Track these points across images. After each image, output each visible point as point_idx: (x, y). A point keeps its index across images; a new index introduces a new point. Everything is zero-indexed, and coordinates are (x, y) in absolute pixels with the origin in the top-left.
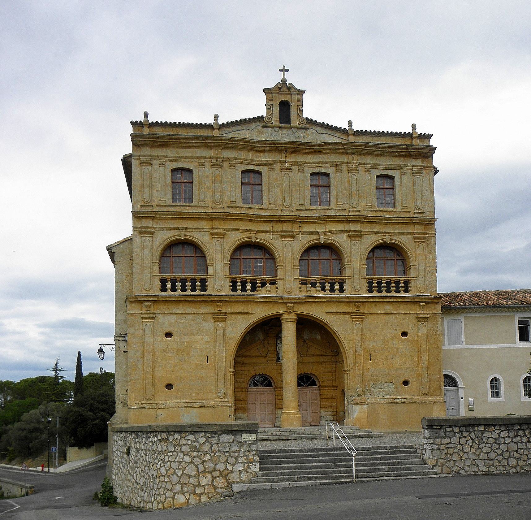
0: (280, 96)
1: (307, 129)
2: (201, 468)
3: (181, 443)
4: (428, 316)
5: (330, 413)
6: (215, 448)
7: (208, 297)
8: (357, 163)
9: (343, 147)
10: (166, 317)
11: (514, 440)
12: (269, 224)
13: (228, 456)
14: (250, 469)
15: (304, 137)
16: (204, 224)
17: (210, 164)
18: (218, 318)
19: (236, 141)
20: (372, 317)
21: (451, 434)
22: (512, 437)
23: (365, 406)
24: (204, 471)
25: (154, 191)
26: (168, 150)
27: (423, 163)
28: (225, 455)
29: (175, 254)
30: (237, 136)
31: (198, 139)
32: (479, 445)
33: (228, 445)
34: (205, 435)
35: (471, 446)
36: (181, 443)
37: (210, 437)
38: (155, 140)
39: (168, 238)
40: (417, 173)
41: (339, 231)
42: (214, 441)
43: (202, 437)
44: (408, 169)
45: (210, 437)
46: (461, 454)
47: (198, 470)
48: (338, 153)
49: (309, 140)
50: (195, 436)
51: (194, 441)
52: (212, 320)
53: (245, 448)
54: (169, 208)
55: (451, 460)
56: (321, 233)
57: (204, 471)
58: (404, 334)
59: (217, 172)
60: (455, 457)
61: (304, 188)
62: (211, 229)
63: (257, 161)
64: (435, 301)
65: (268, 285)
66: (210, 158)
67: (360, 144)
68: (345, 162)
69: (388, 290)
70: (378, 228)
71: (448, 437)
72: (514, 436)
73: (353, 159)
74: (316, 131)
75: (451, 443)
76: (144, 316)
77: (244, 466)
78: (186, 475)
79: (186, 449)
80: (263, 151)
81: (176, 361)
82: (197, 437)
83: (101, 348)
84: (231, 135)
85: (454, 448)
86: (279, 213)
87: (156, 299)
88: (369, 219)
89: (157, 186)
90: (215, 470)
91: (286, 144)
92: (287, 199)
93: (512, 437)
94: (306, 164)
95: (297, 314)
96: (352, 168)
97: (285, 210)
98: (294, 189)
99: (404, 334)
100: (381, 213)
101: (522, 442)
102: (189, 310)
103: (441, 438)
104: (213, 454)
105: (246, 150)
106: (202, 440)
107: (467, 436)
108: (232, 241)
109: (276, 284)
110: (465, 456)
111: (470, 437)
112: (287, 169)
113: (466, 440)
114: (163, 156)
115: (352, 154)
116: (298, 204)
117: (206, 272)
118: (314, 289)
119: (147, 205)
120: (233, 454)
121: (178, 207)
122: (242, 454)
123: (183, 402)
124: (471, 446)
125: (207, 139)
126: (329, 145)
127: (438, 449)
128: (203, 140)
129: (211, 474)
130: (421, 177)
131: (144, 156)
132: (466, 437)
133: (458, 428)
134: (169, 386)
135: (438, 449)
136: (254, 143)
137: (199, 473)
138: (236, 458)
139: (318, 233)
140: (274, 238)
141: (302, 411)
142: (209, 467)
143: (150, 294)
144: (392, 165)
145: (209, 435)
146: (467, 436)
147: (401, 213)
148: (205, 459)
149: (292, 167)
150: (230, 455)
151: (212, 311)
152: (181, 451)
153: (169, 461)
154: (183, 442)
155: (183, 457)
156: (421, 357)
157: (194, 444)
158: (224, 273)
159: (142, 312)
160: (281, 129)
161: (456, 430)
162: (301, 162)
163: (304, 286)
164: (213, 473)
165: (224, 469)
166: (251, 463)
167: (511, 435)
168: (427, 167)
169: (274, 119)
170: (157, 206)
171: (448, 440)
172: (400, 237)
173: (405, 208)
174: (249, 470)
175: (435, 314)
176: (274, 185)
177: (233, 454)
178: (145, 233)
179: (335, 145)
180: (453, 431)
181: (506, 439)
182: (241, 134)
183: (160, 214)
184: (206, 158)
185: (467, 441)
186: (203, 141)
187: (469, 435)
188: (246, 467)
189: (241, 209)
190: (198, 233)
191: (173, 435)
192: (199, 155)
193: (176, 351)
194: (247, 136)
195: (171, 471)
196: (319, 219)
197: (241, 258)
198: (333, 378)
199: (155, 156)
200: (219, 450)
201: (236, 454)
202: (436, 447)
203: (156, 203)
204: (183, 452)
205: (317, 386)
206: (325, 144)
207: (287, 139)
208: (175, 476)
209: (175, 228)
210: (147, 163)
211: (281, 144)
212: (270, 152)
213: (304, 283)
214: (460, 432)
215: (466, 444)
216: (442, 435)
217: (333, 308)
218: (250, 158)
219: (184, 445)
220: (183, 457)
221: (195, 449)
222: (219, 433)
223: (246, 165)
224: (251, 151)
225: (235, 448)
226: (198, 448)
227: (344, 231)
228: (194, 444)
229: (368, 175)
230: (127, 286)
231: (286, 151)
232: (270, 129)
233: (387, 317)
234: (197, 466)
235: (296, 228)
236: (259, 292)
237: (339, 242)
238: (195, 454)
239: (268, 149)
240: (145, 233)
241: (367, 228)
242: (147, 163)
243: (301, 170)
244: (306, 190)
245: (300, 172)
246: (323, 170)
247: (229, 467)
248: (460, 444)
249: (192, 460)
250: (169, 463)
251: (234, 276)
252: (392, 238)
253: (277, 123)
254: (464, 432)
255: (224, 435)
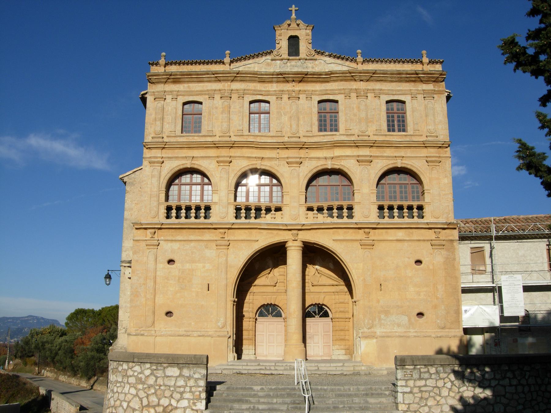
0: (289, 31)
1: (316, 60)
2: (145, 402)
3: (128, 374)
4: (444, 243)
5: (342, 347)
6: (160, 381)
7: (211, 224)
8: (366, 89)
9: (350, 75)
10: (170, 244)
11: (501, 383)
12: (275, 151)
13: (173, 390)
14: (196, 406)
15: (313, 68)
16: (212, 152)
17: (373, 95)
18: (221, 245)
19: (244, 74)
20: (383, 244)
21: (426, 376)
22: (499, 380)
23: (375, 340)
24: (148, 406)
25: (165, 123)
26: (180, 86)
27: (434, 88)
28: (169, 389)
29: (320, 183)
30: (247, 69)
31: (208, 74)
32: (459, 388)
33: (174, 379)
34: (151, 366)
35: (450, 390)
36: (128, 374)
37: (155, 370)
38: (168, 77)
39: (176, 167)
40: (428, 97)
41: (347, 156)
42: (160, 373)
43: (148, 368)
44: (419, 94)
45: (155, 370)
46: (438, 398)
47: (142, 404)
48: (346, 80)
49: (317, 69)
50: (141, 367)
51: (140, 373)
52: (215, 247)
53: (191, 383)
54: (178, 138)
55: (426, 405)
56: (328, 158)
57: (148, 406)
58: (419, 262)
59: (226, 104)
60: (431, 402)
61: (312, 115)
62: (218, 157)
63: (265, 91)
64: (451, 227)
65: (273, 212)
66: (220, 90)
67: (367, 72)
68: (353, 89)
69: (178, 217)
70: (388, 152)
71: (422, 379)
72: (501, 378)
73: (362, 85)
74: (325, 61)
75: (426, 386)
76: (149, 243)
77: (189, 403)
78: (131, 408)
79: (132, 380)
80: (271, 82)
81: (177, 289)
82: (143, 368)
83: (108, 273)
84: (241, 69)
85: (429, 392)
86: (286, 139)
87: (159, 226)
88: (378, 143)
89: (168, 118)
90: (158, 405)
91: (293, 74)
92: (294, 126)
93: (499, 380)
94: (313, 92)
95: (303, 242)
96: (294, 97)
97: (291, 137)
98: (301, 117)
99: (419, 262)
100: (392, 137)
101: (511, 385)
102: (192, 238)
103: (415, 380)
104: (157, 387)
105: (254, 81)
106: (148, 372)
107: (445, 378)
108: (238, 169)
109: (281, 211)
110: (443, 401)
111: (449, 379)
112: (294, 97)
113: (444, 382)
114: (175, 91)
115: (361, 80)
116: (305, 130)
117: (353, 200)
118: (322, 215)
119: (158, 136)
120: (178, 389)
121: (187, 137)
122: (188, 389)
123: (181, 331)
124: (450, 390)
125: (216, 74)
126: (176, 75)
127: (411, 392)
128: (214, 74)
129: (154, 408)
130: (432, 101)
131: (158, 92)
132: (444, 379)
133: (434, 369)
134: (169, 314)
135: (411, 392)
136: (262, 75)
137: (143, 407)
138: (182, 393)
139: (326, 158)
140: (280, 165)
141: (313, 343)
142: (153, 401)
143: (156, 221)
144: (402, 90)
145: (154, 367)
146: (445, 378)
147: (413, 137)
148: (150, 393)
149: (301, 96)
150: (175, 390)
151: (215, 238)
152: (128, 383)
153: (117, 392)
154: (130, 373)
155: (129, 389)
156: (437, 287)
157: (140, 376)
158: (228, 201)
159: (146, 239)
160: (289, 61)
161: (433, 370)
162: (308, 91)
163: (310, 212)
164: (157, 408)
165: (168, 405)
166: (196, 399)
167: (498, 376)
168: (438, 91)
169: (283, 52)
170: (168, 137)
171: (422, 383)
172: (413, 161)
173: (417, 131)
174: (194, 408)
175: (452, 241)
176: (281, 114)
177: (178, 389)
178: (154, 162)
179: (342, 73)
180: (428, 371)
181: (492, 381)
182: (250, 68)
183: (169, 145)
184: (215, 90)
185: (445, 383)
186: (213, 76)
187: (447, 377)
188: (191, 404)
189: (247, 137)
190: (205, 161)
191: (122, 365)
192: (209, 88)
193: (177, 278)
194: (256, 69)
195: (118, 403)
196: (326, 144)
197: (386, 183)
198: (250, 309)
199: (370, 90)
200: (164, 384)
201: (182, 389)
202: (408, 390)
203: (167, 134)
204: (129, 384)
205: (258, 316)
206: (331, 73)
207: (295, 70)
208: (121, 408)
209: (183, 157)
210: (160, 98)
211: (288, 74)
212: (278, 82)
213: (310, 209)
214: (437, 372)
215: (444, 386)
216: (416, 376)
217: (341, 235)
218: (259, 89)
219: (131, 376)
220: (129, 389)
221: (139, 381)
222: (165, 365)
223: (254, 96)
224: (260, 82)
225: (181, 382)
226: (143, 380)
227: (353, 156)
228: (140, 376)
229: (376, 99)
230: (136, 214)
231: (293, 81)
232: (278, 62)
233: (399, 244)
234: (141, 399)
235: (303, 153)
236: (263, 219)
237: (347, 167)
238: (140, 386)
239: (172, 80)
240: (154, 162)
241: (375, 152)
242: (160, 98)
243: (377, 96)
244: (313, 117)
245: (308, 100)
246: (331, 97)
247: (174, 403)
248: (436, 387)
249: (137, 392)
250: (117, 394)
251: (381, 203)
252: (404, 162)
253: (286, 56)
254: (442, 373)
255: (169, 368)
